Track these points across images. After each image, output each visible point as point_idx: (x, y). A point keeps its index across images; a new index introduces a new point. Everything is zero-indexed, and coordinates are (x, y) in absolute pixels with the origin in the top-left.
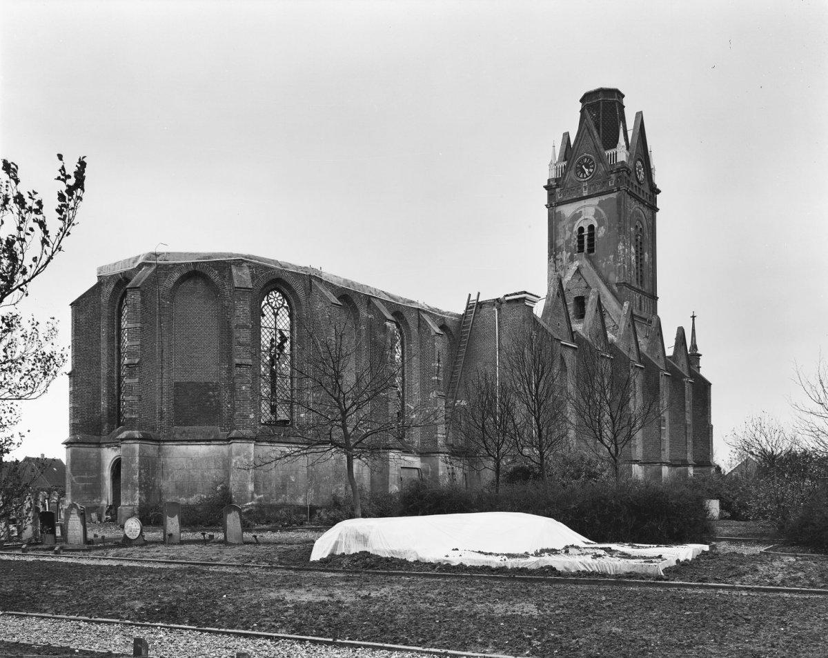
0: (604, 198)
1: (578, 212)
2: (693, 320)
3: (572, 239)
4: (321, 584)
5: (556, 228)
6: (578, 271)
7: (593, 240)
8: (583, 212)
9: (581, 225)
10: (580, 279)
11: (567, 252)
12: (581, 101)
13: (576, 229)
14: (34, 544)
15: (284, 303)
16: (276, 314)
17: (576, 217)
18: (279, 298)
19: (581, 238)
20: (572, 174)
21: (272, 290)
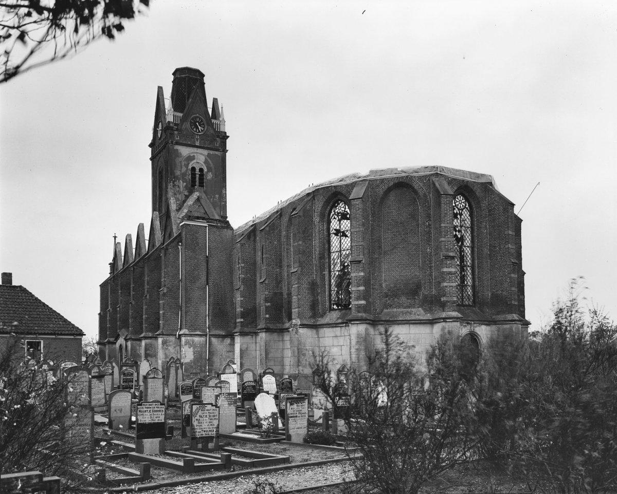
0: (212, 152)
1: (192, 155)
2: (115, 239)
3: (187, 173)
4: (364, 469)
6: (198, 199)
7: (203, 179)
8: (196, 157)
10: (199, 206)
11: (183, 182)
12: (173, 74)
13: (190, 167)
14: (233, 471)
15: (466, 205)
17: (190, 158)
18: (463, 201)
19: (193, 175)
20: (187, 125)
21: (459, 195)
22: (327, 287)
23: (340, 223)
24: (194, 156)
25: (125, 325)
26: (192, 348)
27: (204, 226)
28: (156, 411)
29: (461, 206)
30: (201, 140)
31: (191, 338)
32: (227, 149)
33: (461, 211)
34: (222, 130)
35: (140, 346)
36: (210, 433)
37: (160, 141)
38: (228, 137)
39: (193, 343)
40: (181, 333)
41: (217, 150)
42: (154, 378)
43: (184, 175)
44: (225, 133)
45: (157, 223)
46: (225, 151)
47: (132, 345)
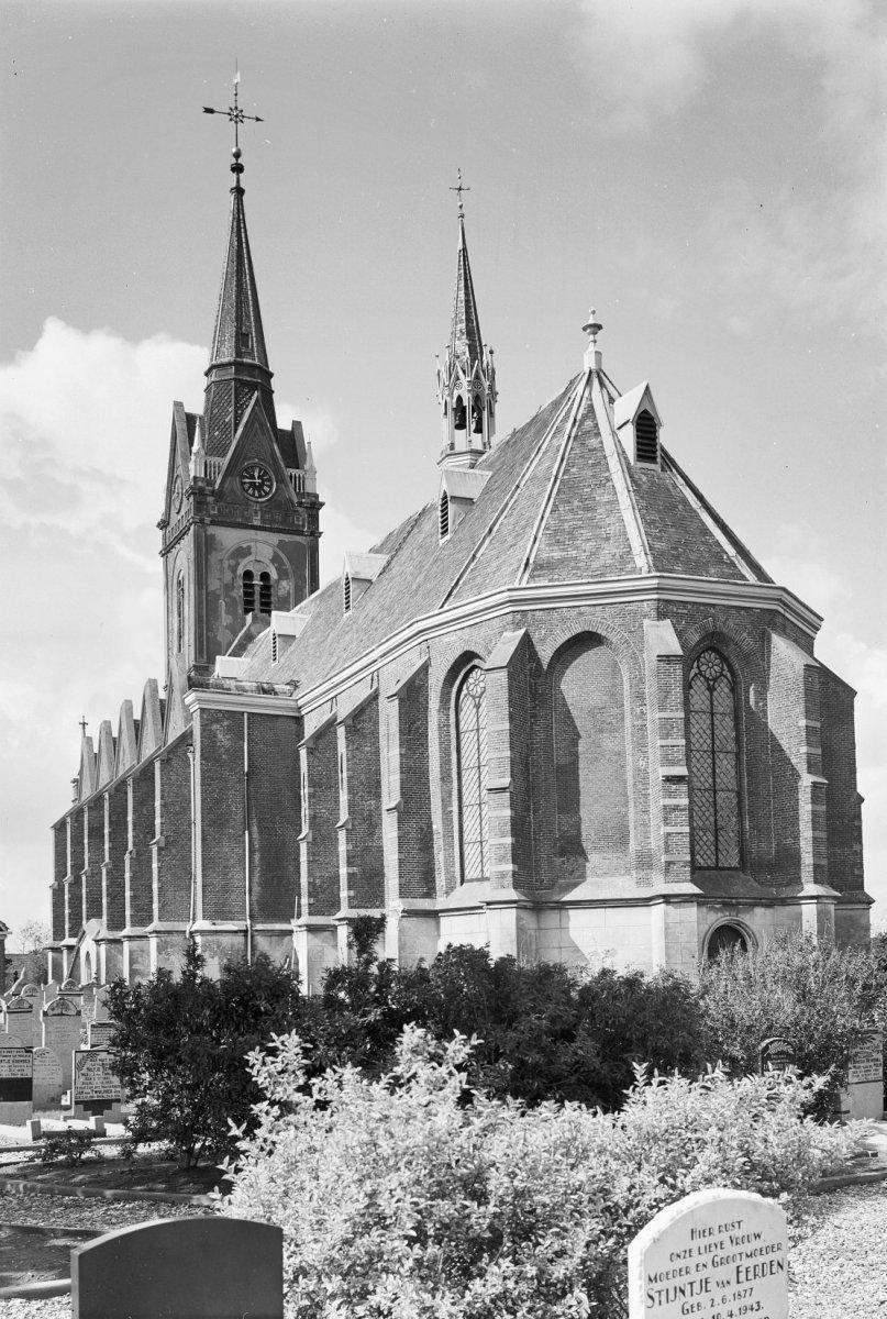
0: (287, 538)
2: (84, 728)
5: (207, 560)
7: (269, 596)
9: (250, 568)
13: (240, 571)
16: (711, 689)
17: (241, 552)
19: (248, 587)
22: (456, 835)
23: (477, 712)
24: (249, 547)
25: (95, 912)
26: (216, 958)
27: (239, 712)
28: (18, 1061)
29: (713, 672)
30: (263, 513)
31: (215, 938)
32: (320, 530)
33: (712, 683)
34: (308, 490)
35: (121, 952)
36: (105, 1095)
37: (179, 517)
38: (322, 504)
39: (218, 947)
40: (195, 928)
41: (300, 533)
42: (62, 1014)
43: (229, 587)
44: (317, 496)
45: (124, 719)
46: (315, 534)
47: (108, 952)
